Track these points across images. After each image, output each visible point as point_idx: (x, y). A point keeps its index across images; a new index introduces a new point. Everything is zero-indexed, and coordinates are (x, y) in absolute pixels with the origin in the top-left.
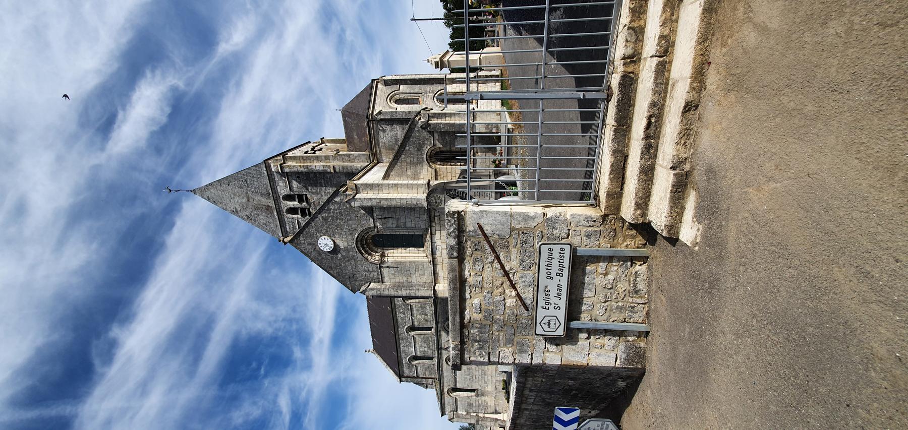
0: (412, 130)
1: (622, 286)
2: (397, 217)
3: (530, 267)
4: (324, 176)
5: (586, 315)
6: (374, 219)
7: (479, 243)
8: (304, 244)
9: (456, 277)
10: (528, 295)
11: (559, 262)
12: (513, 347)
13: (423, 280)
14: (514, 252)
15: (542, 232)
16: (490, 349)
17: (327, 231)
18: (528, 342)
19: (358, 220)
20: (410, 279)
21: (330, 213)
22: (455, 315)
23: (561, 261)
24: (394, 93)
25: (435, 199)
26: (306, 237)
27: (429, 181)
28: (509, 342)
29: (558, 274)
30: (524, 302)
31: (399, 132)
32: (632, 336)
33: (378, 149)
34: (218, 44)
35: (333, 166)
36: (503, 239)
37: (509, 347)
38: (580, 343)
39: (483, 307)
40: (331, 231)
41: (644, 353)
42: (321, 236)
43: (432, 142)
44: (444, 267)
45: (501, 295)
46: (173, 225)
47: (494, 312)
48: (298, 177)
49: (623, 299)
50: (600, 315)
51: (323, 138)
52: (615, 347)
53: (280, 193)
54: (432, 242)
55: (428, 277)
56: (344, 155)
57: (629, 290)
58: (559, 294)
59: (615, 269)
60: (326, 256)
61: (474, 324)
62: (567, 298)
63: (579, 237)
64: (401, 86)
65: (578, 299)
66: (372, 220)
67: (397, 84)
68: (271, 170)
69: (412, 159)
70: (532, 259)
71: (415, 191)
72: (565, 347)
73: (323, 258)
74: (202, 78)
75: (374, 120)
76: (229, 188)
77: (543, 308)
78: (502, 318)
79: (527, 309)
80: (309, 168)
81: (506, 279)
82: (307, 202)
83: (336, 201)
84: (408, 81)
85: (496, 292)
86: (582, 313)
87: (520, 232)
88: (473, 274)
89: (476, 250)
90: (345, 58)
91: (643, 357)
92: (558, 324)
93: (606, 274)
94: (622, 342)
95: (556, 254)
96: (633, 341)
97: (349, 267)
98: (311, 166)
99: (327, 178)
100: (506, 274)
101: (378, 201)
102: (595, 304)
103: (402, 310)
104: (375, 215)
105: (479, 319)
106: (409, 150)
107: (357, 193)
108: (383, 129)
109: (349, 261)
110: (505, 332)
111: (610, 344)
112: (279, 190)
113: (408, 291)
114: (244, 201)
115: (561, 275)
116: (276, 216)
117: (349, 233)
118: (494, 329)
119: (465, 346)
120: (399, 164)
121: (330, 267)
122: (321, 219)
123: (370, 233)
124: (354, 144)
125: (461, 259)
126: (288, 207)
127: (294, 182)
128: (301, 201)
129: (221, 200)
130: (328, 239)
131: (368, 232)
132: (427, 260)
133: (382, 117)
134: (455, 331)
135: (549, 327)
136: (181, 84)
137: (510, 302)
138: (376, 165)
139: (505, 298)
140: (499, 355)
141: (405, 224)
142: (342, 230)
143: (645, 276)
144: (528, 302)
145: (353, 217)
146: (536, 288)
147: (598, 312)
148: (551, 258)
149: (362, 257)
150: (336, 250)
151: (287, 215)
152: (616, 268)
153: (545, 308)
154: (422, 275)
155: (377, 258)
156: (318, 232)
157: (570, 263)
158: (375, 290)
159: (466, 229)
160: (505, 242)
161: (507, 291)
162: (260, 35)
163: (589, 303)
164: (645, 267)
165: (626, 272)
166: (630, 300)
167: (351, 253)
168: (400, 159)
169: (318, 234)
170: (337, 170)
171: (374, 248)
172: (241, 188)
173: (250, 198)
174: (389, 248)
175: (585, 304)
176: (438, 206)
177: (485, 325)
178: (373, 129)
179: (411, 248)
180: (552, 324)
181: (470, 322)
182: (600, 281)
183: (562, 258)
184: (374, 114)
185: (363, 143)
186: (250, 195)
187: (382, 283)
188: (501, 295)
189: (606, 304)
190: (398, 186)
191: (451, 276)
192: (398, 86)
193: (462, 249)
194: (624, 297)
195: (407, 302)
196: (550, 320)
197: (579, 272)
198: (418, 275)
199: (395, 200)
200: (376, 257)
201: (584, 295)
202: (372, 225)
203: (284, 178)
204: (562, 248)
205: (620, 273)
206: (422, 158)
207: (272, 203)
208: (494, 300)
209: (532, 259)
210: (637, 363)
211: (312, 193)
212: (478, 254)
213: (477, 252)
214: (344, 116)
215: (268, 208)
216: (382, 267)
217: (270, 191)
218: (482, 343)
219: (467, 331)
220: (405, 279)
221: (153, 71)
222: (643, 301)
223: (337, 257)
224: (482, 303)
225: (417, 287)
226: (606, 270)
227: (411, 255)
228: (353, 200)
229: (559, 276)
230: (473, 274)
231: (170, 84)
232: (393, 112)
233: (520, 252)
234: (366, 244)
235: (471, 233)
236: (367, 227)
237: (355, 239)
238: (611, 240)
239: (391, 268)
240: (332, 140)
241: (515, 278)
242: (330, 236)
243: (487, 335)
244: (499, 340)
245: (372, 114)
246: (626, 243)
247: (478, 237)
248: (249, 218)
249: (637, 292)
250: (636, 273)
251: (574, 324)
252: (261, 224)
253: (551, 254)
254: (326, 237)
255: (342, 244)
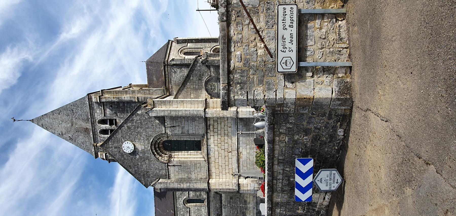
0: (196, 65)
1: (332, 37)
2: (182, 125)
3: (273, 27)
4: (130, 105)
5: (310, 59)
6: (165, 127)
7: (240, 11)
8: (112, 147)
9: (225, 35)
10: (272, 46)
11: (290, 17)
12: (264, 86)
13: (200, 176)
14: (262, 16)
15: (279, 2)
16: (248, 89)
17: (130, 137)
18: (273, 81)
19: (154, 128)
20: (190, 176)
21: (133, 123)
22: (224, 63)
23: (292, 16)
24: (183, 48)
25: (211, 86)
26: (114, 142)
27: (206, 99)
28: (261, 82)
29: (290, 26)
30: (269, 51)
31: (185, 71)
32: (341, 73)
33: (170, 85)
34: (61, 33)
35: (138, 97)
36: (254, 8)
37: (261, 87)
38: (307, 80)
39: (243, 57)
40: (133, 137)
41: (351, 86)
42: (125, 141)
43: (209, 74)
44: (216, 165)
45: (254, 47)
46: (6, 160)
47: (250, 60)
48: (111, 106)
49: (333, 46)
50: (319, 58)
51: (131, 84)
52: (331, 82)
53: (96, 118)
54: (207, 145)
55: (204, 174)
56: (146, 90)
57: (336, 39)
58: (291, 41)
59: (326, 24)
60: (127, 157)
61: (237, 70)
62: (296, 43)
63: (302, 4)
64: (188, 44)
65: (304, 47)
66: (164, 128)
67: (186, 43)
68: (92, 101)
69: (194, 86)
70: (273, 20)
71: (196, 106)
72: (297, 84)
73: (125, 159)
74: (46, 54)
75: (169, 65)
76: (59, 116)
77: (282, 51)
78: (255, 64)
79: (272, 57)
80: (120, 99)
81: (257, 35)
82: (116, 125)
83: (138, 114)
84: (193, 41)
85: (252, 45)
86: (308, 57)
87: (266, 2)
88: (236, 33)
89: (238, 16)
90: (148, 48)
91: (350, 89)
92: (292, 63)
93: (321, 28)
94: (335, 79)
95: (288, 12)
96: (342, 77)
97: (144, 166)
98: (121, 97)
99: (132, 107)
100: (258, 32)
101: (169, 112)
102: (315, 50)
103: (182, 213)
104: (166, 124)
105: (240, 67)
106: (193, 80)
107: (154, 107)
108: (175, 71)
109: (144, 160)
110: (258, 75)
111: (327, 81)
112: (96, 116)
113: (188, 184)
114: (68, 125)
115: (292, 26)
116: (92, 136)
117: (146, 139)
118: (250, 73)
119: (231, 88)
120: (185, 90)
121: (130, 166)
122: (126, 128)
123: (161, 139)
124: (153, 85)
125: (228, 25)
126: (101, 129)
127: (108, 110)
128: (111, 124)
129: (52, 126)
130: (130, 143)
131: (160, 138)
132: (204, 159)
133: (174, 63)
134: (224, 75)
135: (286, 66)
136: (31, 58)
137: (261, 52)
138: (168, 96)
139: (258, 49)
140: (254, 93)
141: (188, 131)
142: (141, 136)
143: (345, 27)
144: (272, 51)
145: (150, 125)
146: (277, 41)
147: (318, 56)
148: (285, 15)
149: (154, 157)
150: (135, 152)
151: (100, 135)
152: (326, 24)
153: (283, 52)
154: (199, 172)
155: (166, 159)
156: (123, 138)
157: (297, 18)
158: (163, 184)
159: (231, 3)
160: (256, 10)
161: (258, 44)
162: (90, 30)
163: (312, 49)
164: (344, 22)
165: (333, 26)
166: (338, 45)
167: (146, 154)
168: (186, 85)
169: (123, 140)
170: (140, 100)
171: (164, 151)
172: (68, 115)
173: (74, 123)
174: (175, 152)
175: (309, 51)
176: (212, 92)
177: (244, 71)
178: (168, 71)
179: (192, 151)
180: (288, 63)
181: (234, 69)
182: (317, 33)
183: (292, 15)
184: (169, 61)
185: (160, 83)
186: (74, 121)
187: (169, 179)
188: (254, 47)
189: (322, 50)
190: (184, 102)
191: (222, 34)
192: (187, 44)
193: (229, 16)
194: (333, 45)
195: (187, 205)
196: (286, 60)
197: (304, 28)
198: (196, 172)
199: (181, 111)
200: (165, 158)
201: (308, 44)
202: (164, 132)
203: (100, 107)
204: (292, 8)
205: (330, 27)
206: (202, 85)
207: (90, 126)
208: (250, 51)
209: (273, 20)
210: (346, 94)
211: (120, 118)
212: (239, 19)
213: (238, 18)
214: (148, 65)
215: (86, 130)
216: (170, 166)
217: (90, 117)
218: (242, 84)
219: (232, 76)
220: (186, 175)
221: (12, 48)
222: (345, 46)
223: (135, 158)
224: (242, 54)
225: (195, 181)
226: (320, 25)
227: (191, 156)
228: (151, 111)
229: (291, 27)
230: (236, 33)
231: (22, 58)
232: (182, 59)
233: (266, 16)
234: (158, 148)
235: (235, 5)
236: (160, 133)
237: (150, 143)
238: (322, 4)
239: (176, 167)
240: (137, 85)
241: (263, 34)
242: (132, 141)
243: (246, 78)
244: (253, 82)
245: (167, 61)
246: (331, 6)
247: (239, 7)
248: (71, 138)
249: (341, 39)
250: (339, 26)
251: (302, 64)
252: (80, 143)
253: (285, 12)
254: (129, 142)
255: (140, 147)
